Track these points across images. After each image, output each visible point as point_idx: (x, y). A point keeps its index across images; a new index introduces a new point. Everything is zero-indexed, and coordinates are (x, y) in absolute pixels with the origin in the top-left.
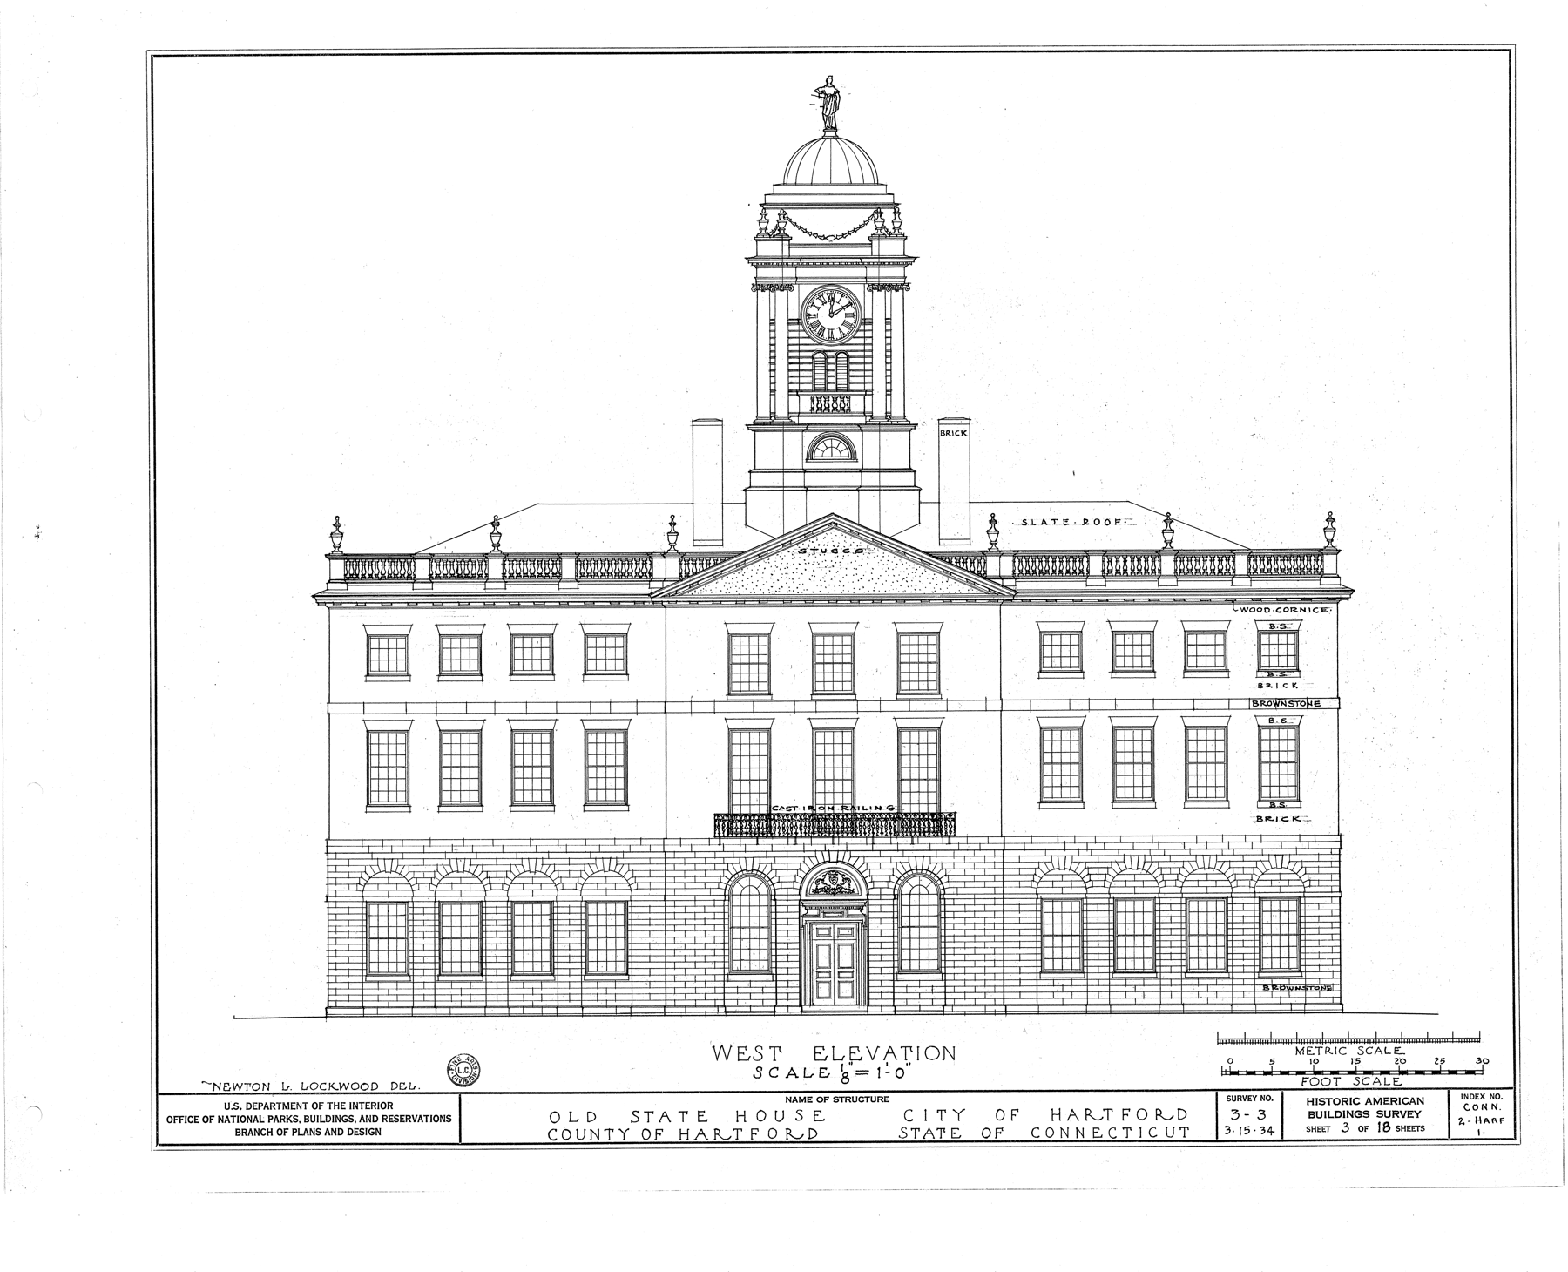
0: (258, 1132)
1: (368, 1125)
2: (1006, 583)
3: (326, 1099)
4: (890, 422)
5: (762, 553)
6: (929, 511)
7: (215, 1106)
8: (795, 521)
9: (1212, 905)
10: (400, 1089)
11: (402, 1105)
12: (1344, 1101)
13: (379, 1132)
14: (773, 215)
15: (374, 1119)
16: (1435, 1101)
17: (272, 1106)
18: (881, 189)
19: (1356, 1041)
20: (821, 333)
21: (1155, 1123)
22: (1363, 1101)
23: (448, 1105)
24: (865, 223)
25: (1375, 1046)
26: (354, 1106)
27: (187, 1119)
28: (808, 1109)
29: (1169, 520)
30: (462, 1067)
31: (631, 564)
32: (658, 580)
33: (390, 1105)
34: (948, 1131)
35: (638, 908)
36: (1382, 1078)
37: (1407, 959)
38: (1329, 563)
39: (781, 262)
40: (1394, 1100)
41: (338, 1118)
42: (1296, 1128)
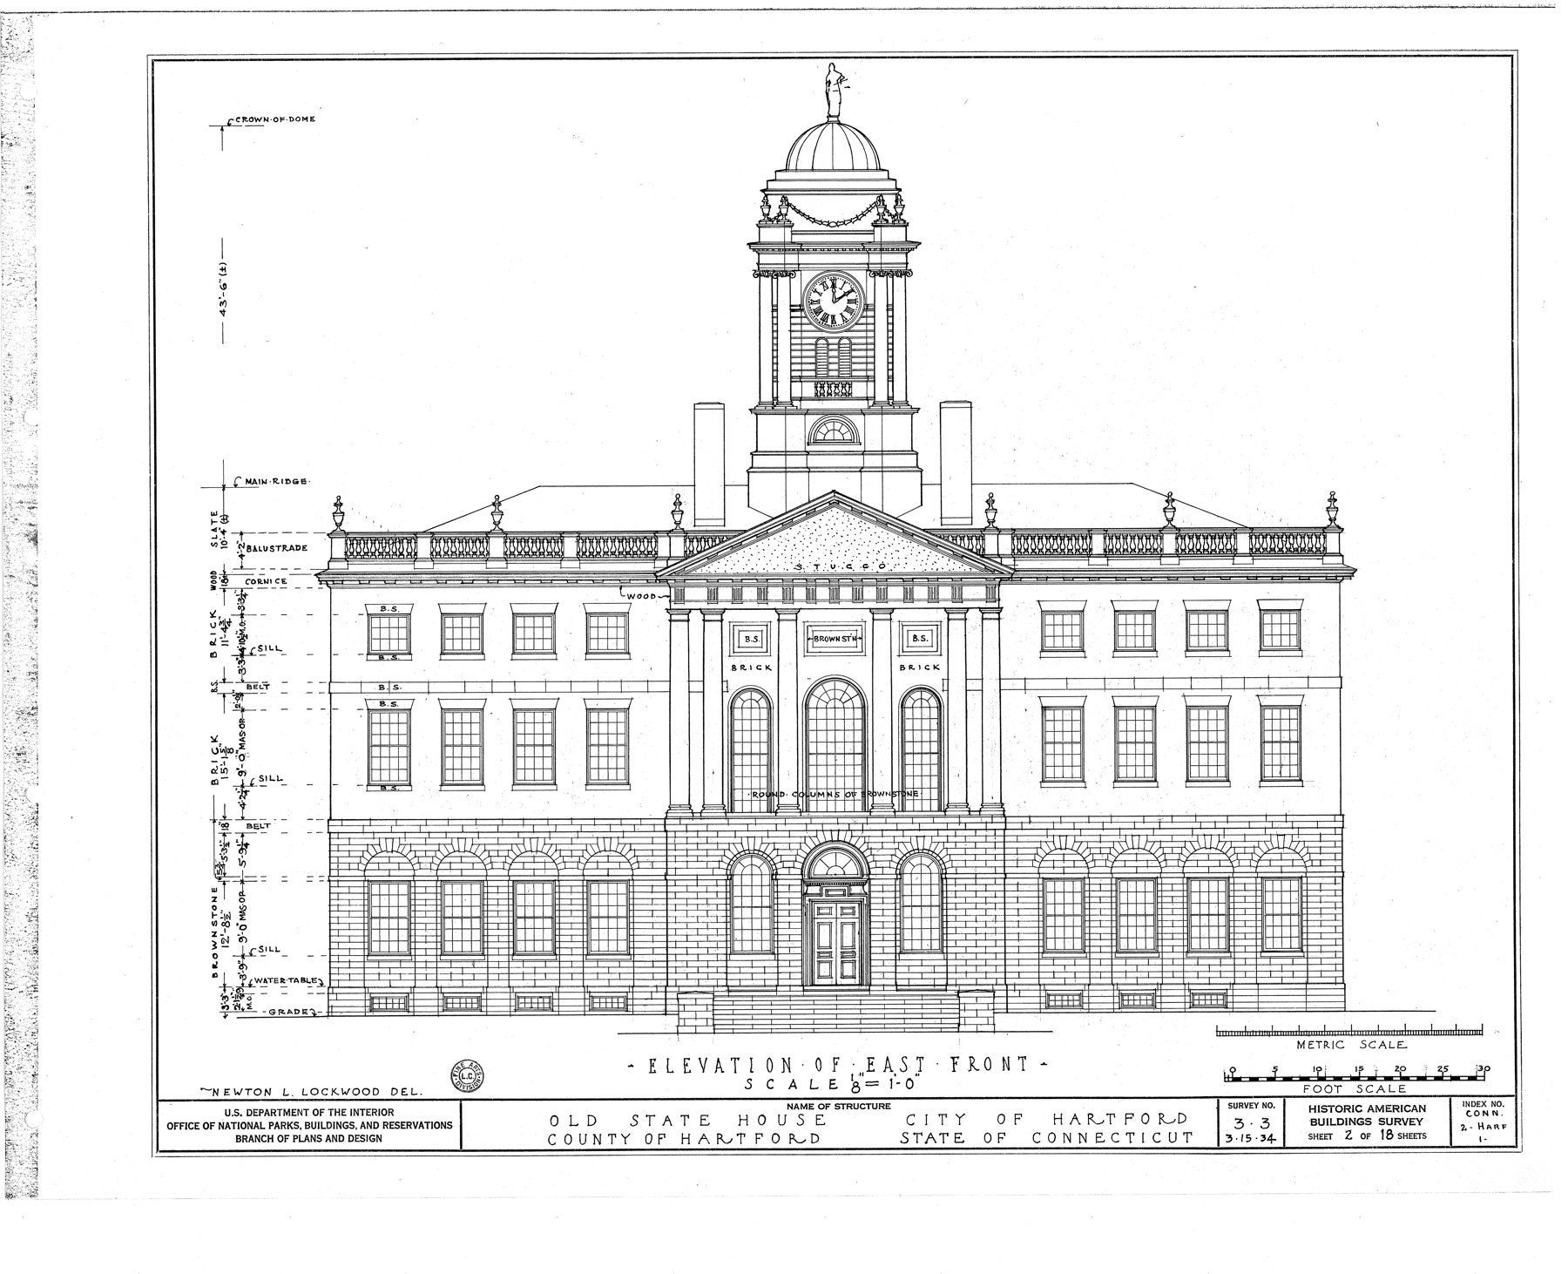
0: (259, 1139)
1: (369, 1132)
2: (1005, 561)
3: (326, 1105)
4: (892, 406)
5: (761, 533)
6: (931, 493)
7: (216, 1112)
8: (797, 499)
9: (1213, 884)
10: (405, 1096)
11: (403, 1112)
12: (1346, 1108)
13: (379, 1138)
14: (775, 201)
15: (374, 1125)
16: (1437, 1108)
17: (273, 1113)
18: (884, 175)
19: (1361, 1033)
20: (824, 319)
21: (1159, 1128)
22: (1365, 1109)
23: (449, 1112)
24: (868, 210)
25: (1379, 1039)
26: (355, 1112)
27: (188, 1126)
28: (809, 1115)
29: (1170, 499)
30: (465, 1073)
31: (636, 544)
32: (662, 558)
33: (391, 1112)
34: (952, 1136)
35: (640, 888)
36: (1386, 1084)
37: (1411, 946)
38: (1332, 542)
39: (784, 248)
40: (1396, 1108)
41: (340, 1125)
42: (1298, 1136)
